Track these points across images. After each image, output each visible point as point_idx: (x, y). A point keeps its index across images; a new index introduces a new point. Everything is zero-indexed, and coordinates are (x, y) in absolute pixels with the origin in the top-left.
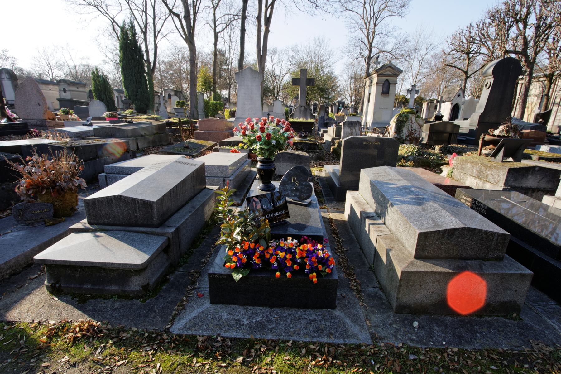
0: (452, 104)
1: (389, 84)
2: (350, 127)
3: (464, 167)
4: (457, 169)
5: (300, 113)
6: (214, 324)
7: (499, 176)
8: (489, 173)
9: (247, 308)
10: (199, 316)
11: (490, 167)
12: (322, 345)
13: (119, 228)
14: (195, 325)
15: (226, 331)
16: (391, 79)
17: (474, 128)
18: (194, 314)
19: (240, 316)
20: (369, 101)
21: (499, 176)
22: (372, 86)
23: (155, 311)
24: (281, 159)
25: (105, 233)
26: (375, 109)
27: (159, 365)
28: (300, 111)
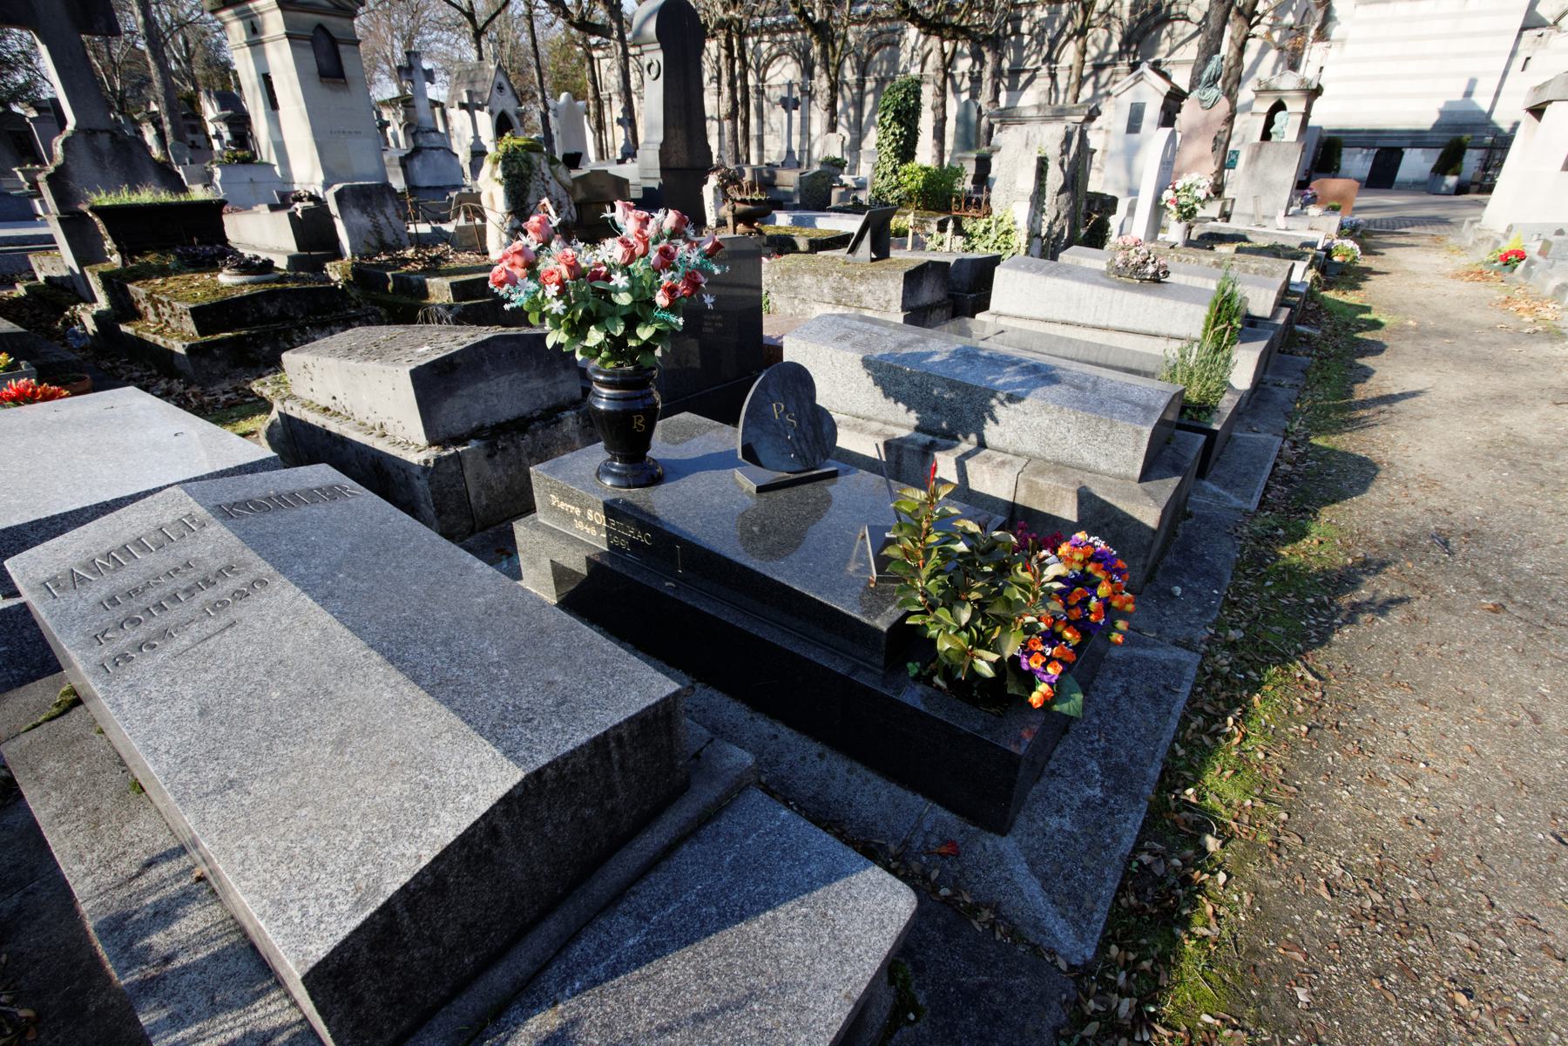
0: (491, 113)
1: (334, 43)
2: (364, 210)
3: (794, 284)
4: (779, 292)
5: (100, 165)
6: (1085, 853)
7: (886, 292)
8: (862, 289)
9: (1053, 772)
10: (1045, 879)
11: (862, 276)
12: (1192, 707)
13: (553, 926)
14: (1075, 898)
15: (1117, 839)
16: (334, 23)
17: (655, 184)
18: (1033, 887)
19: (1076, 796)
20: (272, 103)
21: (886, 292)
22: (269, 47)
23: (984, 986)
24: (487, 367)
25: (566, 986)
26: (316, 133)
27: (1207, 1018)
28: (96, 153)
